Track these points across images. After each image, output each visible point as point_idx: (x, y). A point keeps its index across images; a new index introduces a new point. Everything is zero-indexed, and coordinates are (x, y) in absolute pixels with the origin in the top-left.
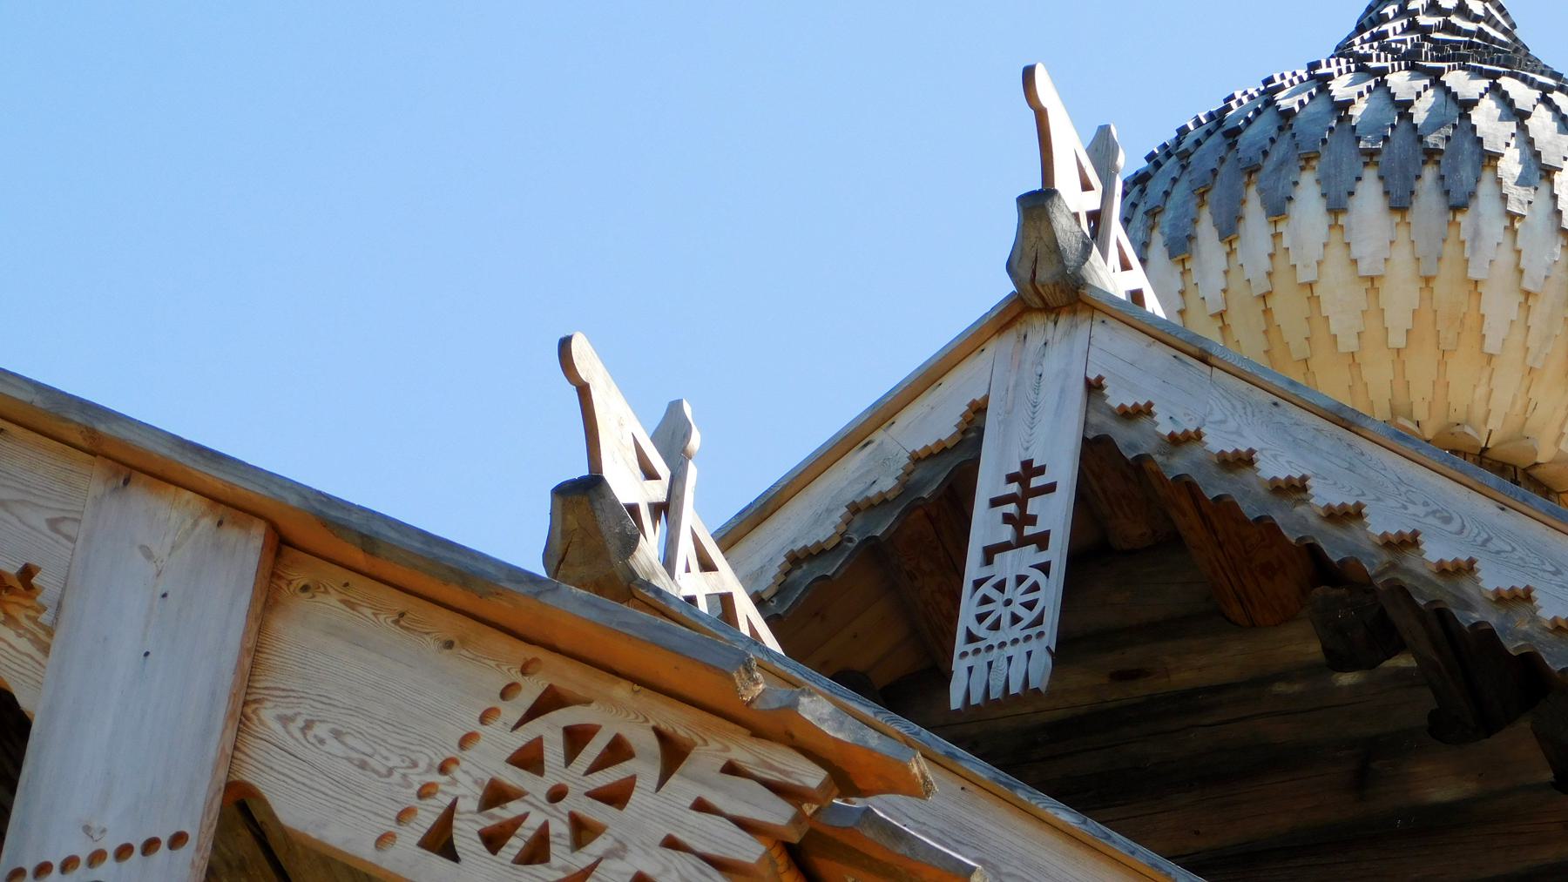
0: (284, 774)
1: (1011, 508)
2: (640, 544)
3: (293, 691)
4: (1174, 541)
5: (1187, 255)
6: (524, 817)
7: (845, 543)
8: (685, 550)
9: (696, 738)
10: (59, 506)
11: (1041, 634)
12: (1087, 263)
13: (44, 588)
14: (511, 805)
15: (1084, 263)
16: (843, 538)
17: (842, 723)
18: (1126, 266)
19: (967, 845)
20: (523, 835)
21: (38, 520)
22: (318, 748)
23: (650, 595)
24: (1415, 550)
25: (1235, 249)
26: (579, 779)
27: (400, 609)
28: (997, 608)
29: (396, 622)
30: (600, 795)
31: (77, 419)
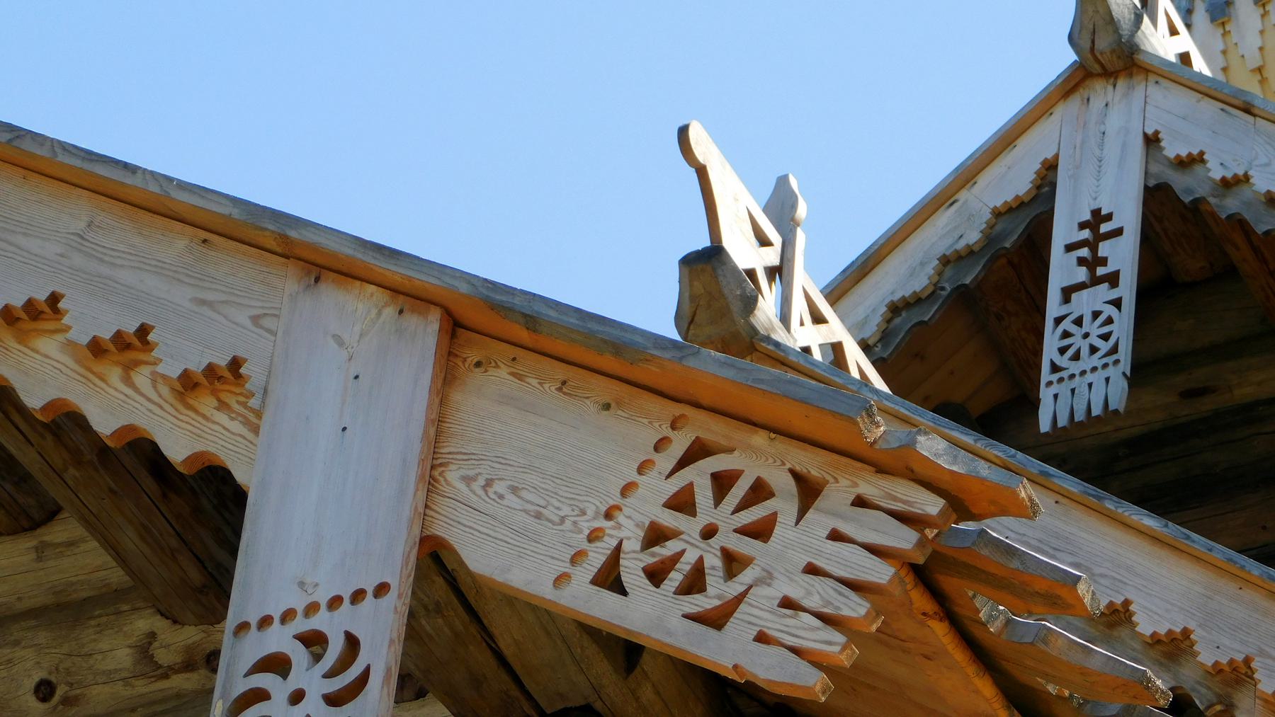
0: (470, 527)
1: (1084, 252)
2: (759, 304)
3: (474, 454)
4: (1230, 272)
5: (1226, 19)
6: (683, 552)
7: (938, 292)
8: (799, 308)
9: (828, 478)
10: (260, 304)
11: (1117, 362)
12: (1139, 32)
13: (251, 377)
14: (669, 543)
15: (1137, 32)
16: (936, 287)
17: (955, 457)
18: (1173, 32)
19: (1063, 551)
20: (682, 570)
21: (243, 317)
22: (498, 503)
23: (771, 347)
24: (1202, 165)
25: (1268, 11)
26: (727, 518)
27: (561, 377)
28: (1077, 341)
29: (560, 389)
30: (745, 531)
31: (271, 227)
